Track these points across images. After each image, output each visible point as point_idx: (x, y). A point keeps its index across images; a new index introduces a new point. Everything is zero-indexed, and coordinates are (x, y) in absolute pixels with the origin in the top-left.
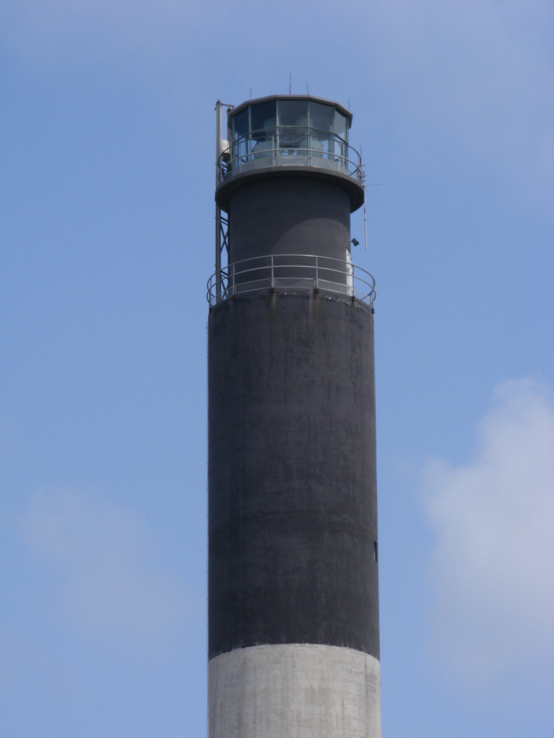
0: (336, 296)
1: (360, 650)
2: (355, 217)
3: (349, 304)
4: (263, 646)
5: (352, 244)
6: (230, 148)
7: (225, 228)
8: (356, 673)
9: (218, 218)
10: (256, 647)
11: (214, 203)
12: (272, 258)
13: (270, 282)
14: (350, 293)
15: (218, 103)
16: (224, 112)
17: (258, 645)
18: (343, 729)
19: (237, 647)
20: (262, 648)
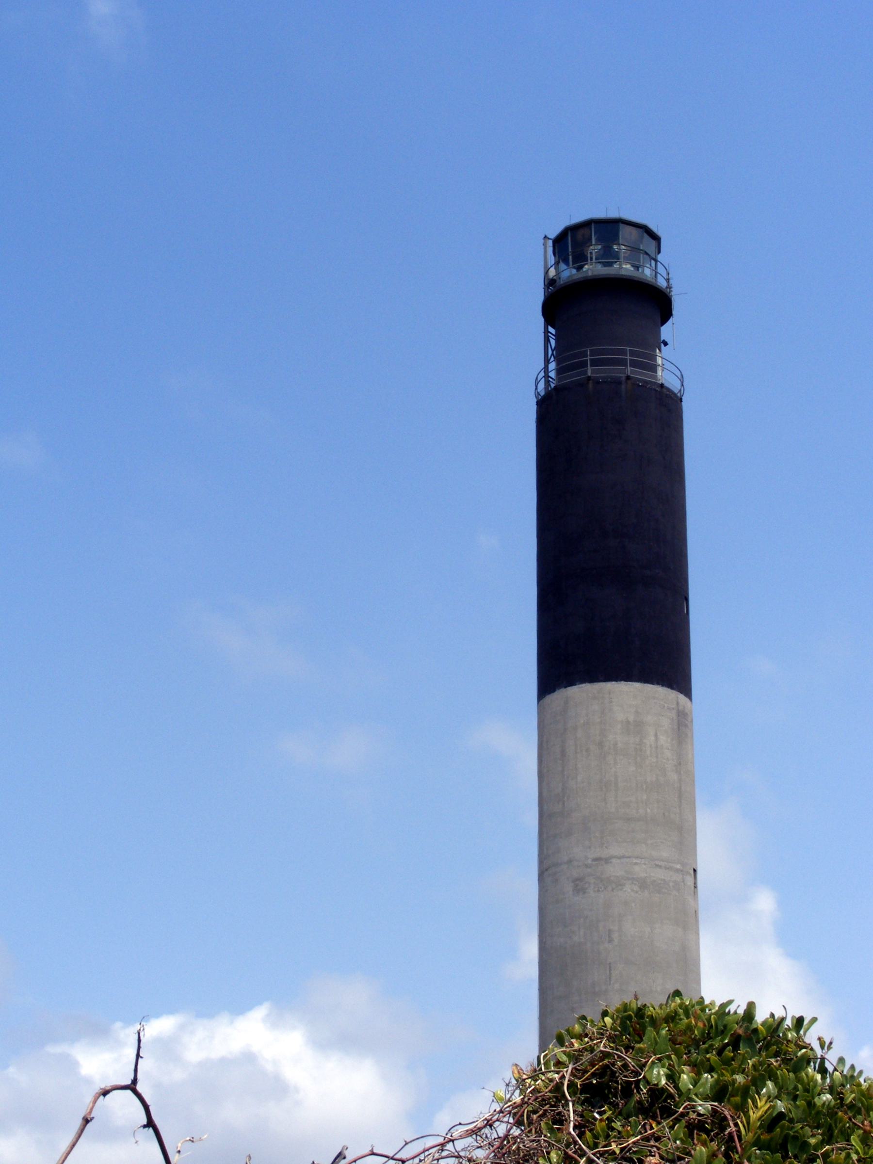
1: (672, 688)
2: (666, 331)
3: (659, 390)
4: (583, 685)
5: (662, 345)
6: (555, 263)
7: (553, 342)
8: (668, 708)
9: (546, 332)
10: (577, 686)
11: (542, 320)
12: (589, 351)
13: (586, 371)
15: (546, 237)
16: (550, 243)
17: (579, 684)
18: (657, 757)
20: (582, 687)
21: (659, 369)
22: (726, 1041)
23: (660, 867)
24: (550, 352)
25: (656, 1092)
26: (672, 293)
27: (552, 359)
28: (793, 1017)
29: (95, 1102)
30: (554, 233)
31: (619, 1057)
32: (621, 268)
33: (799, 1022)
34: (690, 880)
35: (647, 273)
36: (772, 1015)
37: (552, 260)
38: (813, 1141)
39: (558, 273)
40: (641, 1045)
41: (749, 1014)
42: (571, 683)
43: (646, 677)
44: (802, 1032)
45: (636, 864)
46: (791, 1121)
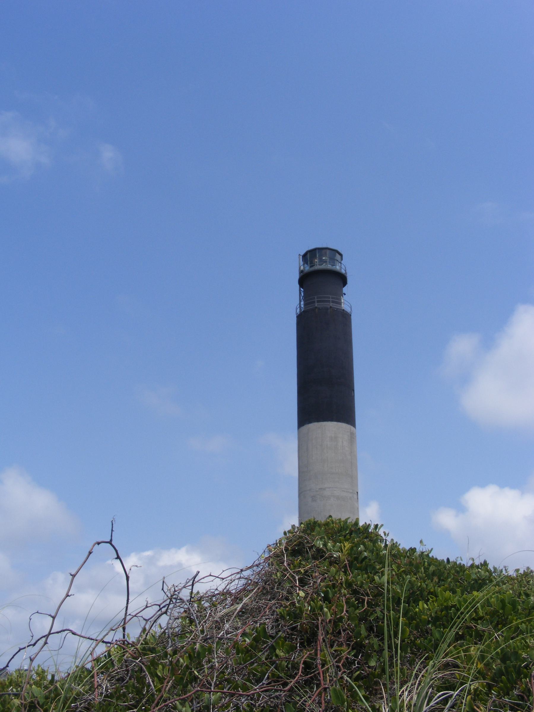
0: (338, 309)
2: (345, 290)
5: (344, 295)
7: (302, 294)
9: (300, 290)
11: (298, 286)
14: (343, 309)
15: (299, 255)
16: (301, 257)
19: (306, 424)
21: (342, 304)
22: (347, 532)
23: (344, 491)
24: (301, 298)
25: (319, 550)
26: (347, 275)
27: (302, 300)
28: (374, 524)
29: (94, 546)
30: (302, 253)
31: (305, 538)
32: (328, 266)
33: (376, 526)
34: (355, 496)
35: (337, 268)
36: (366, 523)
37: (302, 263)
38: (378, 567)
39: (304, 268)
40: (314, 533)
41: (356, 523)
42: (310, 422)
43: (338, 420)
44: (377, 530)
45: (335, 490)
46: (370, 560)
